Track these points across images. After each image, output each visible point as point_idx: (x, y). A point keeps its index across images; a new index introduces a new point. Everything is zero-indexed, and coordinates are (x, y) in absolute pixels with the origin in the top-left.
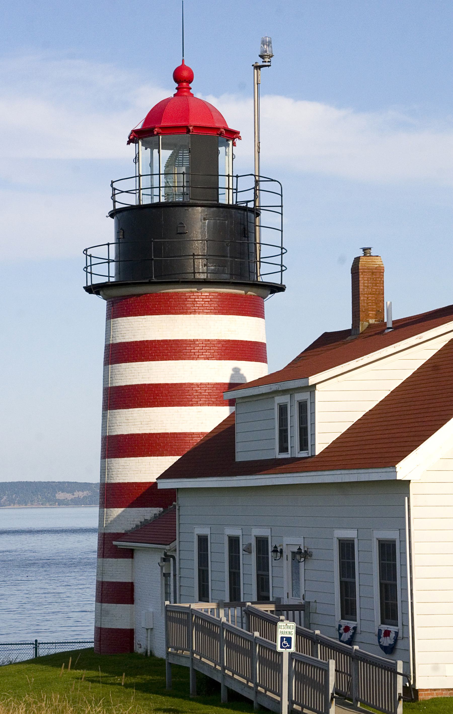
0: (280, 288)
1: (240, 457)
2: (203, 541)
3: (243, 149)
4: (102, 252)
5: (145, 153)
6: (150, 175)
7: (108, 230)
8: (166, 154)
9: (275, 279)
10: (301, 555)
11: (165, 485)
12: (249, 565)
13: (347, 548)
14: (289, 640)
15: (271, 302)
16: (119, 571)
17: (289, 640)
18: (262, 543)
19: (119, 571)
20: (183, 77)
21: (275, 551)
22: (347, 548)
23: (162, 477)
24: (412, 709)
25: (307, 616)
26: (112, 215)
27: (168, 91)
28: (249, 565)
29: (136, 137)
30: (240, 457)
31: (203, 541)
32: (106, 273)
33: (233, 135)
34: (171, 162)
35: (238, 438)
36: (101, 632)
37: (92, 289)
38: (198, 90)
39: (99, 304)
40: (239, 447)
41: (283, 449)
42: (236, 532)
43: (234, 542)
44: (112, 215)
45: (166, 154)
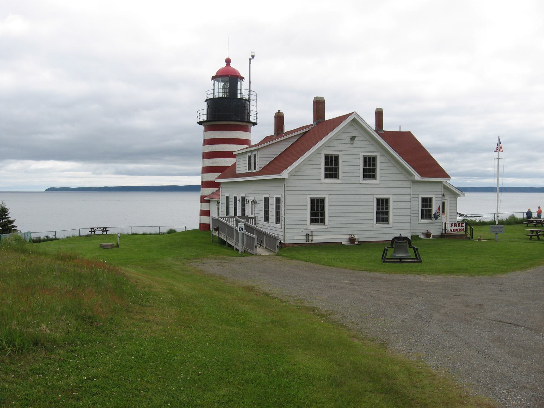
0: (255, 124)
1: (237, 172)
2: (227, 198)
3: (245, 83)
4: (202, 112)
5: (217, 83)
6: (218, 90)
7: (205, 105)
8: (222, 84)
9: (255, 121)
10: (254, 202)
11: (217, 181)
12: (239, 205)
13: (266, 200)
14: (242, 228)
15: (253, 128)
16: (206, 207)
17: (242, 228)
18: (243, 198)
19: (206, 207)
20: (228, 61)
21: (246, 201)
22: (266, 200)
23: (216, 179)
24: (171, 290)
25: (255, 221)
26: (206, 101)
27: (224, 65)
28: (239, 205)
29: (214, 78)
30: (237, 172)
31: (227, 198)
32: (205, 118)
33: (242, 78)
34: (224, 86)
35: (237, 166)
36: (201, 224)
37: (200, 123)
38: (232, 65)
39: (202, 127)
40: (237, 169)
41: (249, 169)
42: (236, 195)
43: (235, 198)
44: (206, 101)
45: (222, 84)
